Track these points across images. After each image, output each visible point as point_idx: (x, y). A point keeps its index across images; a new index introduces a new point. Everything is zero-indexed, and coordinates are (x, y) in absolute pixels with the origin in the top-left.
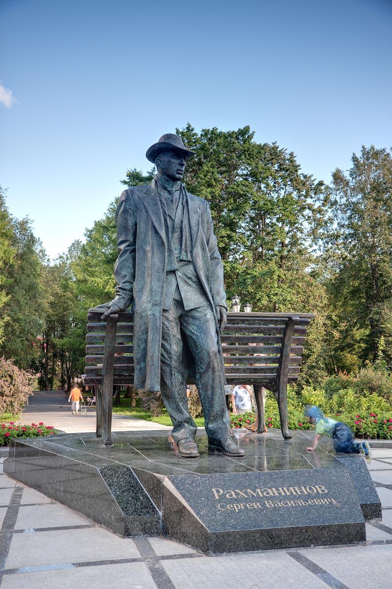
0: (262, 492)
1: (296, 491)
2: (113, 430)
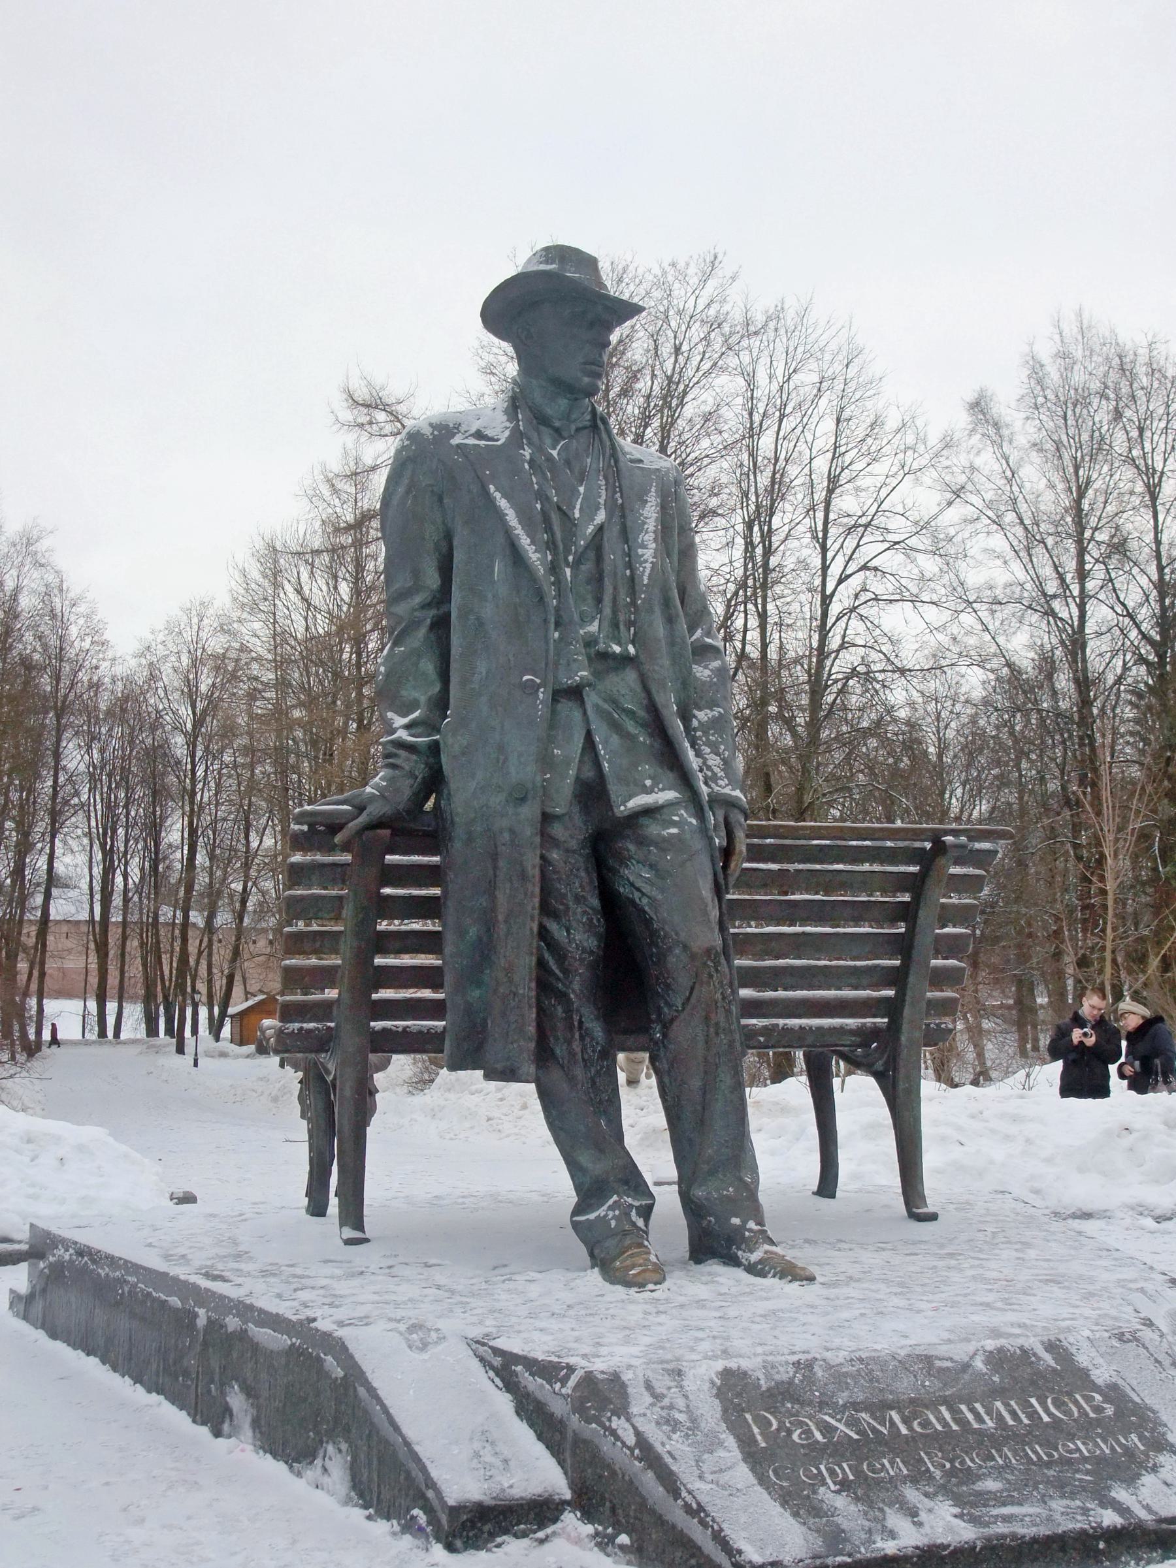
0: (907, 1421)
1: (1014, 1414)
2: (337, 991)
